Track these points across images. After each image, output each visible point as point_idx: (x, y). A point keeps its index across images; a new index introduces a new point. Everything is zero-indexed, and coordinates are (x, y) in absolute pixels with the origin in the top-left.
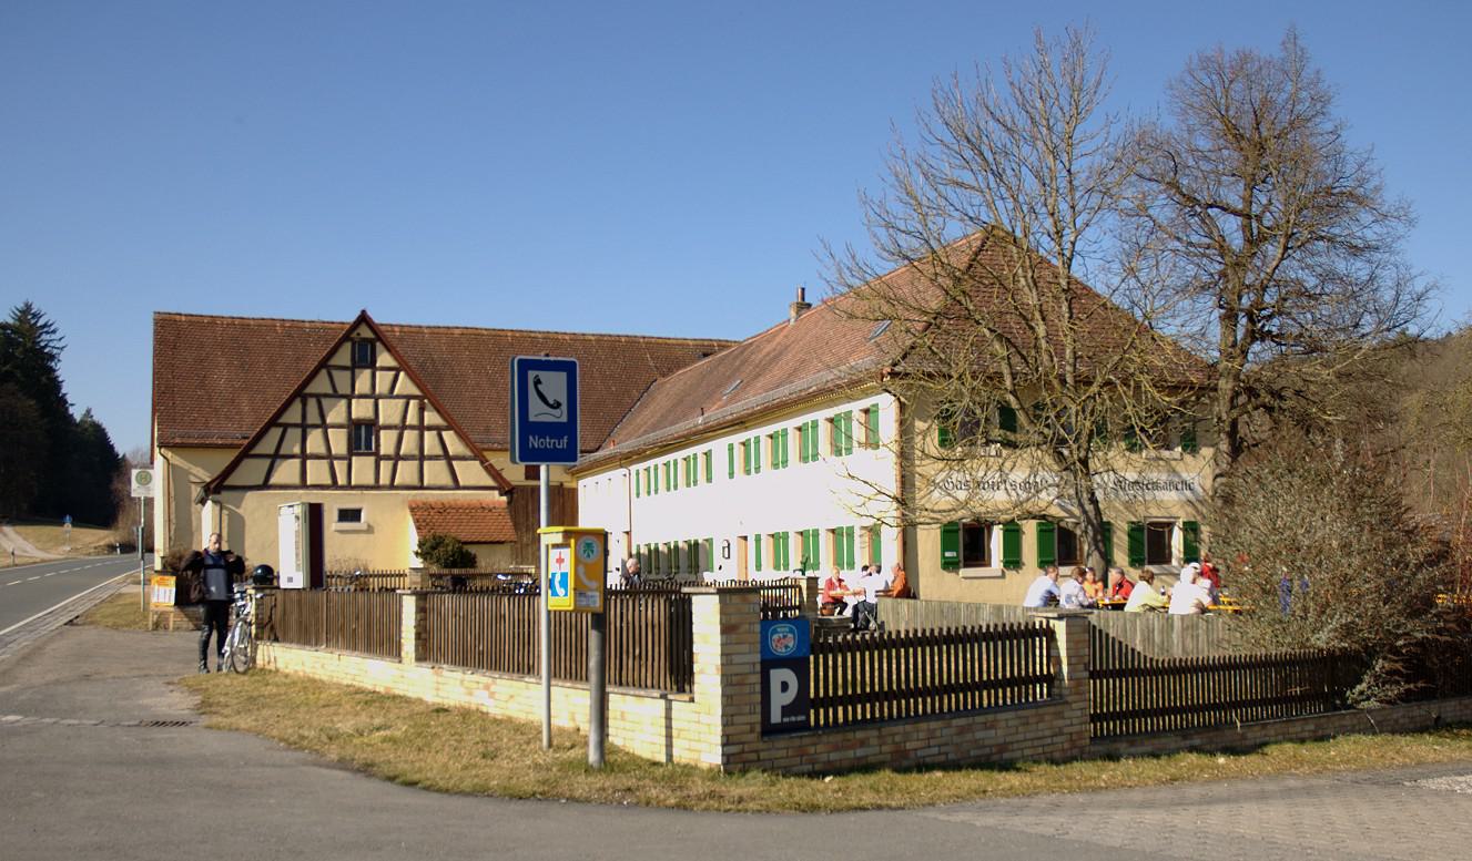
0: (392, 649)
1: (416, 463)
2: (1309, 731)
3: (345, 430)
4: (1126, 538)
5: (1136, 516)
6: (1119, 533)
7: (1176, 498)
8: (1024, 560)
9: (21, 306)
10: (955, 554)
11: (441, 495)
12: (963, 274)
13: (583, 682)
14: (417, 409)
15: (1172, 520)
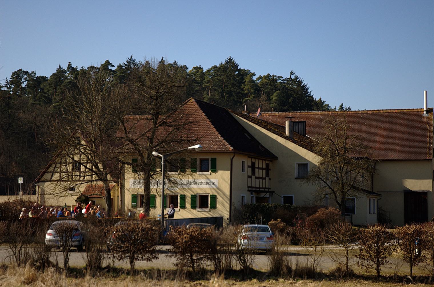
0: (261, 224)
4: (190, 200)
5: (193, 193)
6: (188, 198)
7: (208, 187)
8: (157, 206)
9: (249, 70)
10: (135, 204)
12: (338, 163)
15: (207, 194)
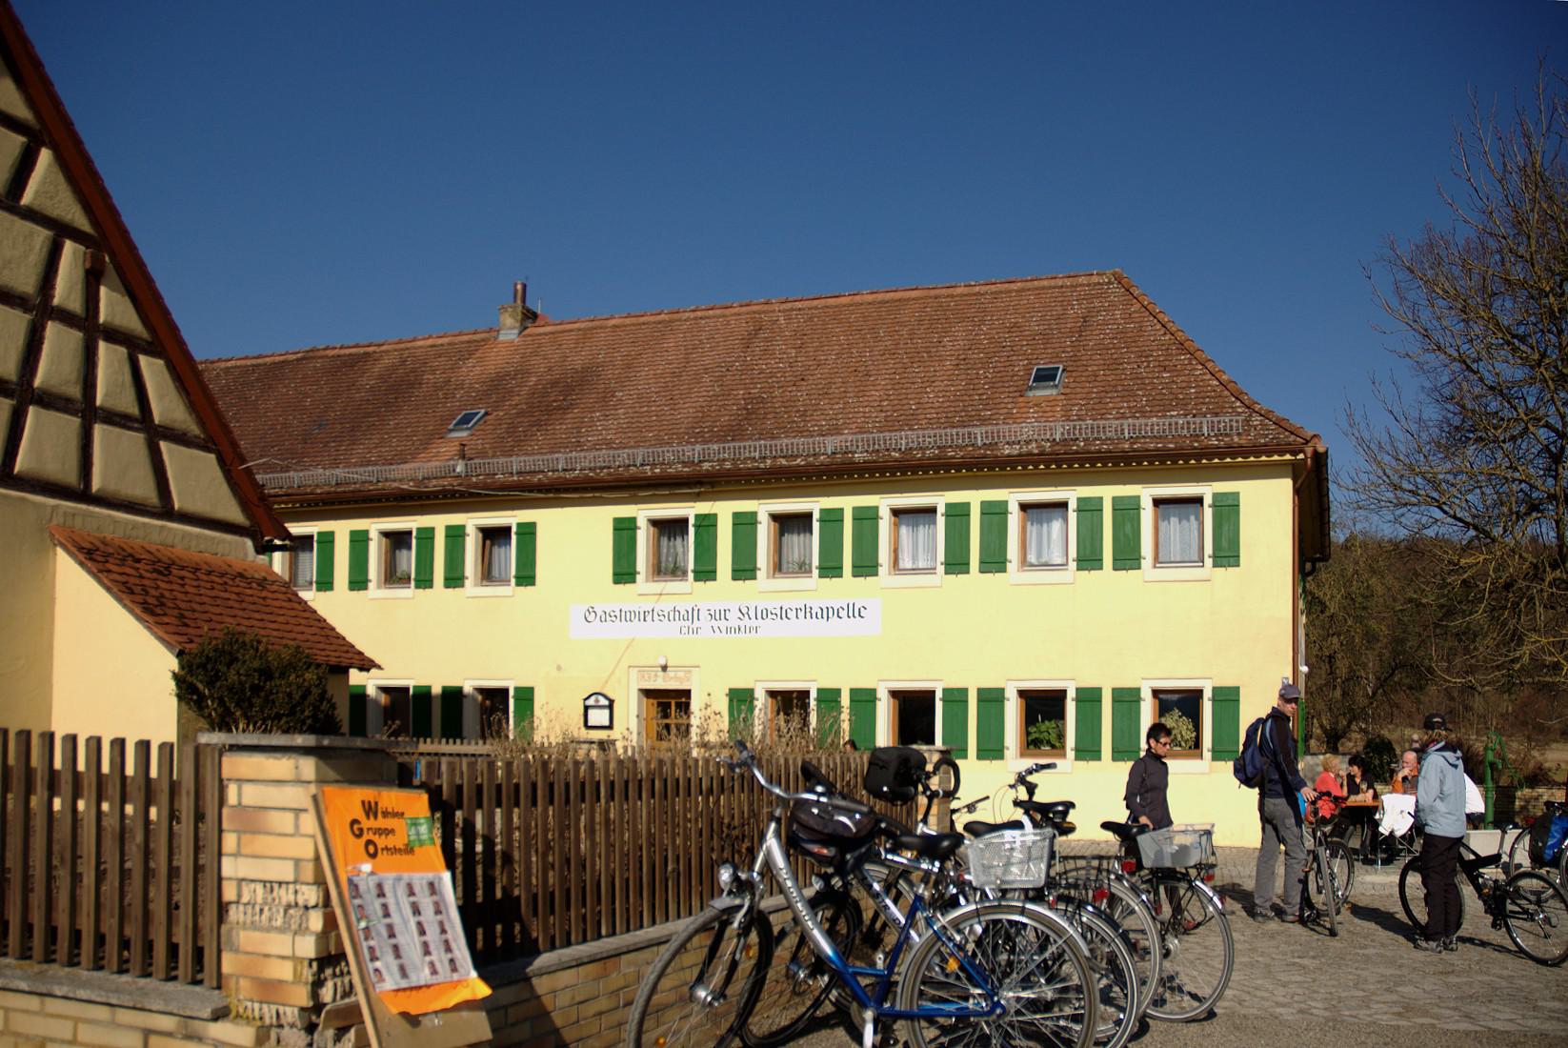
1: (75, 422)
2: (430, 831)
3: (22, 139)
11: (135, 526)
13: (84, 974)
14: (80, 273)
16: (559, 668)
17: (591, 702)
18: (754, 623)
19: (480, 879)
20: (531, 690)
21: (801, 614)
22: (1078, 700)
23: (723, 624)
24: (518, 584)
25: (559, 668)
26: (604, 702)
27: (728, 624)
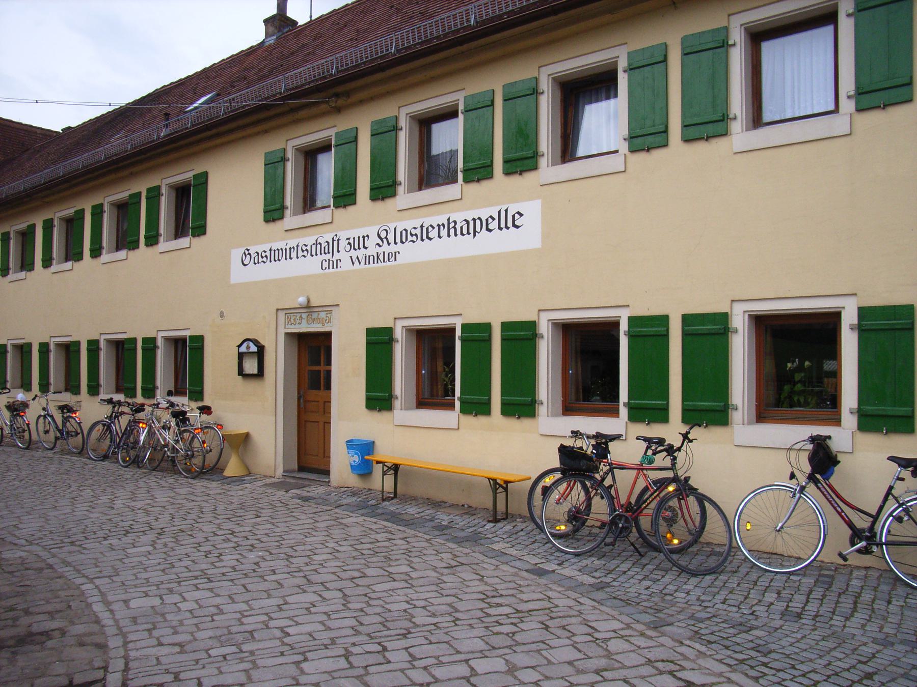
16: (222, 315)
17: (243, 349)
18: (393, 248)
19: (196, 105)
20: (198, 343)
21: (444, 232)
22: (862, 330)
23: (361, 253)
24: (467, 181)
25: (222, 315)
26: (254, 348)
27: (368, 252)
